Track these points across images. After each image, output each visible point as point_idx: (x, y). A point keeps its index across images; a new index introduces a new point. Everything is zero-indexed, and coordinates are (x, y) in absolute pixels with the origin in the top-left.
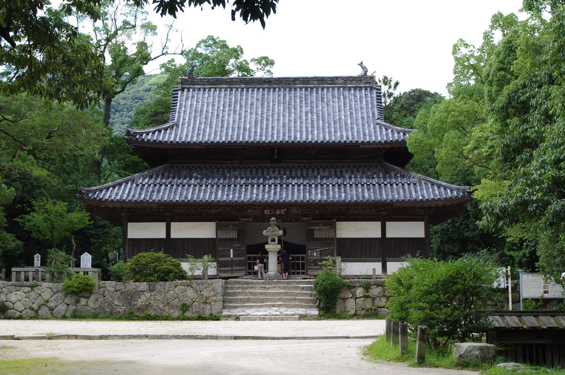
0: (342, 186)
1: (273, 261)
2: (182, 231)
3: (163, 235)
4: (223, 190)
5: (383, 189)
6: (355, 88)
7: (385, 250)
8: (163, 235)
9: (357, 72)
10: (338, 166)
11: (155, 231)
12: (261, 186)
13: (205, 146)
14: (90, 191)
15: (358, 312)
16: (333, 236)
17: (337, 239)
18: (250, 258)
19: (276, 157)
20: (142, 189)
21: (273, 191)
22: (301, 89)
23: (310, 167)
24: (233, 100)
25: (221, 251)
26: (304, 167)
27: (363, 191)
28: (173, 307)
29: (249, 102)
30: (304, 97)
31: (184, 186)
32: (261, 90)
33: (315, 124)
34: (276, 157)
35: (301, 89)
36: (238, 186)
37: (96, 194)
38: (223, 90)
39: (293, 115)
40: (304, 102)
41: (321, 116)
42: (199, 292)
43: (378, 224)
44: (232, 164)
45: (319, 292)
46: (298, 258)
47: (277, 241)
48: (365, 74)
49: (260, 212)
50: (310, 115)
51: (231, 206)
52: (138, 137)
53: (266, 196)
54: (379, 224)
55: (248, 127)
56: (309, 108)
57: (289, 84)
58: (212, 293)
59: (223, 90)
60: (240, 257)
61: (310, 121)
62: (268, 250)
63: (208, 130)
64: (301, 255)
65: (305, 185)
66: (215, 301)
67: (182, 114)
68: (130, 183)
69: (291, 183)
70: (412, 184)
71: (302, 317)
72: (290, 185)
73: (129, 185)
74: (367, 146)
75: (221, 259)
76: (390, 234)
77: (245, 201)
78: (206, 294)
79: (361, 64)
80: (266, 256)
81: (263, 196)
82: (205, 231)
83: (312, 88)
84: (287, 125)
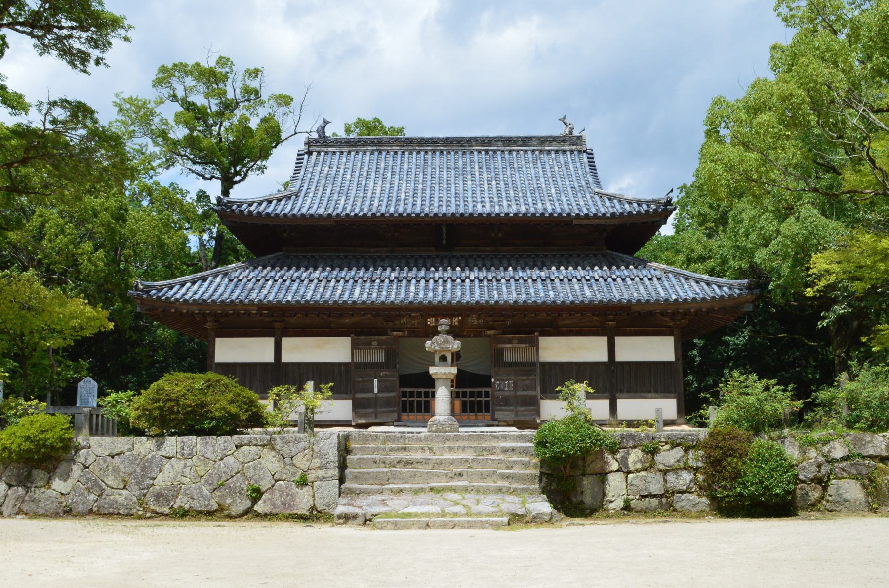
0: (548, 281)
1: (442, 397)
2: (300, 350)
3: (269, 358)
4: (363, 287)
5: (612, 285)
6: (556, 152)
7: (613, 380)
8: (269, 358)
9: (560, 130)
10: (538, 256)
11: (256, 350)
12: (423, 281)
13: (336, 222)
14: (152, 287)
15: (633, 504)
16: (534, 360)
17: (544, 364)
18: (404, 394)
19: (444, 242)
20: (236, 286)
21: (440, 288)
22: (479, 152)
23: (496, 257)
24: (382, 165)
25: (359, 382)
26: (487, 256)
27: (582, 289)
28: (232, 491)
29: (406, 167)
30: (484, 162)
31: (303, 281)
32: (422, 153)
33: (504, 194)
34: (444, 242)
35: (479, 152)
36: (387, 281)
37: (163, 291)
38: (368, 153)
39: (469, 183)
40: (484, 168)
41: (510, 185)
42: (288, 460)
43: (603, 341)
44: (377, 252)
45: (543, 462)
46: (479, 394)
47: (449, 359)
48: (571, 133)
49: (419, 319)
50: (494, 183)
51: (374, 309)
52: (234, 207)
53: (431, 294)
54: (604, 340)
55: (403, 196)
56: (493, 174)
57: (462, 146)
58: (317, 462)
59: (368, 153)
60: (390, 392)
61: (495, 190)
62: (434, 377)
63: (342, 201)
64: (483, 390)
65: (491, 280)
66: (322, 479)
67: (307, 182)
68: (220, 276)
69: (468, 277)
70: (655, 279)
71: (516, 519)
72: (467, 280)
73: (218, 279)
74: (585, 222)
75: (359, 396)
76: (621, 356)
77: (397, 302)
78: (301, 462)
79: (563, 120)
80: (430, 390)
81: (426, 295)
82: (335, 350)
83: (495, 152)
84: (461, 195)
